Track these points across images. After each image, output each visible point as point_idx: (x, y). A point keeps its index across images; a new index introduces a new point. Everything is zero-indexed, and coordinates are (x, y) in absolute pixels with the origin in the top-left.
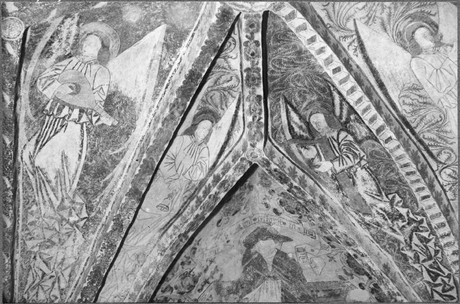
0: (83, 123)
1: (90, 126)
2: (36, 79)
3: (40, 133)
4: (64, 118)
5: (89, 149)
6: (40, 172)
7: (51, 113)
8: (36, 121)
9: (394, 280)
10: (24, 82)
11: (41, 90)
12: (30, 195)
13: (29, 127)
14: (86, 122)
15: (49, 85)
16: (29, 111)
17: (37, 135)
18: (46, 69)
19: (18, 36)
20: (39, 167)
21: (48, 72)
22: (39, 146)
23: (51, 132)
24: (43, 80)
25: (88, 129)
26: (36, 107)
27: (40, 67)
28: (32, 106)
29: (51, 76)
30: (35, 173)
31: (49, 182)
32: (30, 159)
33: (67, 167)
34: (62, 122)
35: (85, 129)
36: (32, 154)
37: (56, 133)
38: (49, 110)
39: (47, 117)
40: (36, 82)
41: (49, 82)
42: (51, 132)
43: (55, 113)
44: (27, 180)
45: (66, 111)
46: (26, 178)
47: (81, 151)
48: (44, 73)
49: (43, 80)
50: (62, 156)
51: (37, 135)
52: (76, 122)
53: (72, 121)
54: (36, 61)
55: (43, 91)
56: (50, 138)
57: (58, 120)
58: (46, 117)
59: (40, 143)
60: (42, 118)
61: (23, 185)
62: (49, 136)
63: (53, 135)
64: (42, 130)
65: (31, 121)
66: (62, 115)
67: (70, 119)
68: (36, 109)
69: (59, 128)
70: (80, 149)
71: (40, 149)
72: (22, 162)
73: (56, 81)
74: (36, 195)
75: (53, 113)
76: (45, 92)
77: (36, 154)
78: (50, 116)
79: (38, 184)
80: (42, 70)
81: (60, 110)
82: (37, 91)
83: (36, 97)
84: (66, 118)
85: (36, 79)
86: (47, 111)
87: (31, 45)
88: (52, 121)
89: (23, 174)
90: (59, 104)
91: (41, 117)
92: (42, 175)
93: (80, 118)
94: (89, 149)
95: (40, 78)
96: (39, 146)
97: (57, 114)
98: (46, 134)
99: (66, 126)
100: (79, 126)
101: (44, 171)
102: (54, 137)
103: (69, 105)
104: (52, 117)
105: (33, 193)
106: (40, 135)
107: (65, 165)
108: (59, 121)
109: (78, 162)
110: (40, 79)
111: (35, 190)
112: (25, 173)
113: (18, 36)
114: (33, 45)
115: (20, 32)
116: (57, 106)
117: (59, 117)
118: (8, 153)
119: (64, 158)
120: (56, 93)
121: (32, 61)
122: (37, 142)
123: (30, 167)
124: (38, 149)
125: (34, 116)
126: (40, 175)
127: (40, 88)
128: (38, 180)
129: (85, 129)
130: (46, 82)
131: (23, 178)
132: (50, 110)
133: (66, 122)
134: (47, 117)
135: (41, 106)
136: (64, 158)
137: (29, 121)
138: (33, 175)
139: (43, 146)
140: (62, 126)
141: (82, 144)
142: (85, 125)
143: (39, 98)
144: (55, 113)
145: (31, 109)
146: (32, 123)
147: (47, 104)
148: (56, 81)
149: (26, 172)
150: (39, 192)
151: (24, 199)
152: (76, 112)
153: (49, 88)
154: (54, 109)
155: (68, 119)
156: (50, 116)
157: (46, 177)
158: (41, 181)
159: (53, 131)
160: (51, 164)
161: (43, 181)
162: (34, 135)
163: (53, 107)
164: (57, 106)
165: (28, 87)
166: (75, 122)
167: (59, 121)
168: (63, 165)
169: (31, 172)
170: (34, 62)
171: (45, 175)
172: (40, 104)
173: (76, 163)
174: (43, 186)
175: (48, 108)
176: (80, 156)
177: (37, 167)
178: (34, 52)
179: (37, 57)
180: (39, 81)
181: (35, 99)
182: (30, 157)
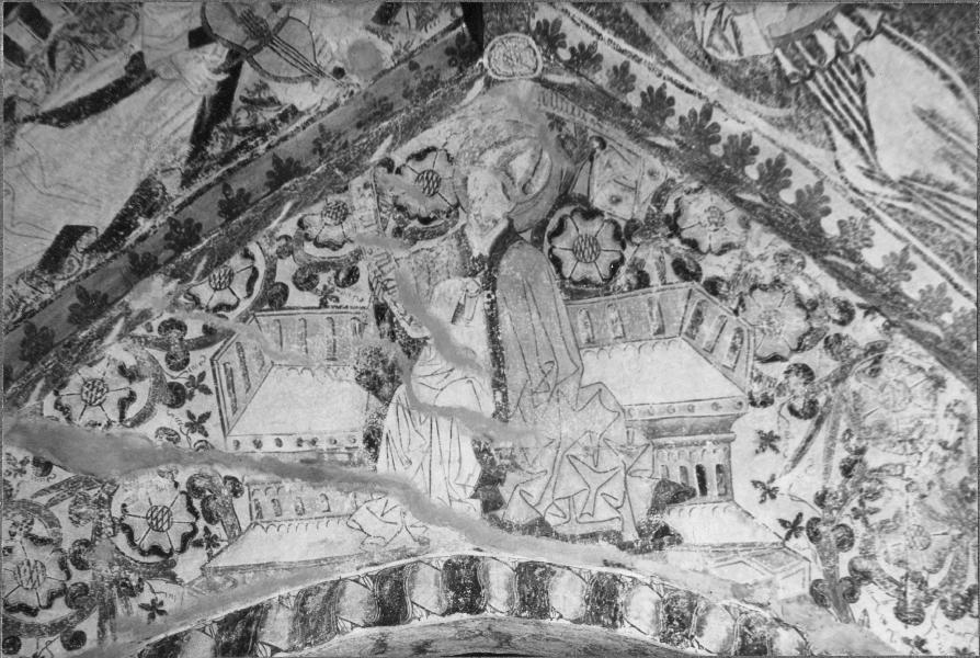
0: (879, 25)
1: (897, 19)
2: (700, 53)
3: (835, 120)
4: (839, 54)
5: (952, 59)
6: (918, 185)
7: (808, 71)
8: (797, 110)
9: (339, 352)
10: (689, 79)
11: (736, 57)
12: (945, 240)
13: (801, 131)
14: (882, 20)
15: (736, 35)
16: (762, 109)
17: (833, 127)
18: (692, 24)
19: (535, 54)
20: (905, 178)
21: (703, 23)
22: (863, 142)
23: (851, 99)
24: (716, 40)
25: (901, 27)
26: (765, 89)
27: (677, 32)
28: (755, 95)
29: (717, 22)
30: (910, 194)
31: (951, 188)
32: (872, 178)
33: (953, 130)
34: (847, 63)
35: (895, 32)
36: (866, 167)
37: (861, 90)
38: (795, 70)
39: (810, 83)
40: (707, 56)
41: (729, 33)
42: (851, 99)
43: (813, 62)
44: (909, 220)
45: (826, 42)
46: (904, 217)
47: (944, 76)
48: (698, 31)
49: (716, 40)
50: (923, 119)
51: (833, 127)
52: (868, 36)
53: (855, 47)
54: (659, 32)
55: (740, 53)
56: (864, 111)
57: (834, 67)
58: (807, 88)
59: (860, 134)
60: (802, 95)
61: (913, 233)
62: (858, 109)
63: (864, 100)
64: (828, 113)
65: (789, 119)
66: (830, 53)
67: (851, 44)
68: (770, 92)
69: (854, 78)
70: (937, 75)
71: (871, 143)
72: (863, 195)
73: (736, 19)
74: (957, 231)
75: (812, 68)
76: (748, 52)
77: (872, 160)
78: (812, 76)
79: (936, 208)
80: (688, 32)
81: (815, 50)
82: (730, 66)
83: (742, 76)
84: (843, 49)
85: (700, 53)
86: (794, 74)
87: (615, 22)
88: (826, 80)
89: (890, 215)
90: (798, 44)
91: (798, 95)
92: (926, 188)
93: (862, 23)
94: (952, 59)
95: (704, 45)
96: (863, 142)
97: (820, 62)
98: (847, 110)
99: (864, 62)
100: (880, 38)
101: (923, 176)
102: (868, 102)
103: (815, 25)
104: (817, 74)
105: (949, 233)
106: (838, 125)
107: (944, 130)
108: (839, 67)
109: (962, 102)
110: (709, 45)
111: (945, 224)
112: (890, 210)
113: (535, 54)
114: (617, 19)
115: (530, 46)
116: (802, 49)
117: (828, 61)
118: (782, 216)
119: (930, 118)
120: (766, 32)
121: (654, 39)
122: (852, 138)
123: (887, 190)
124: (867, 148)
125: (782, 106)
126: (920, 191)
127: (729, 57)
128: (927, 202)
129: (895, 32)
130: (723, 38)
131: (897, 221)
132: (800, 68)
133: (852, 57)
134: (810, 83)
135: (773, 78)
136: (930, 118)
137: (784, 122)
138: (909, 200)
139: (869, 135)
140: (856, 69)
141: (928, 62)
142: (887, 27)
143: (752, 72)
144: (813, 62)
145: (762, 102)
146: (794, 118)
147: (779, 64)
148: (736, 19)
149: (890, 206)
150: (957, 222)
151: (943, 256)
152: (845, 25)
153: (745, 40)
154: (803, 58)
155: (847, 46)
156: (812, 76)
157: (937, 184)
158: (936, 199)
159: (852, 93)
160: (922, 152)
161: (940, 197)
162: (829, 133)
163: (797, 57)
164: (802, 49)
165: (707, 77)
166: (864, 39)
167: (839, 67)
168: (943, 135)
169: (899, 199)
170: (659, 37)
171: (932, 182)
172: (766, 78)
173: (961, 107)
174: (948, 205)
175: (788, 68)
176: (954, 88)
177: (901, 182)
178: (637, 25)
179: (654, 24)
180: (710, 51)
181: (747, 80)
182: (869, 174)
